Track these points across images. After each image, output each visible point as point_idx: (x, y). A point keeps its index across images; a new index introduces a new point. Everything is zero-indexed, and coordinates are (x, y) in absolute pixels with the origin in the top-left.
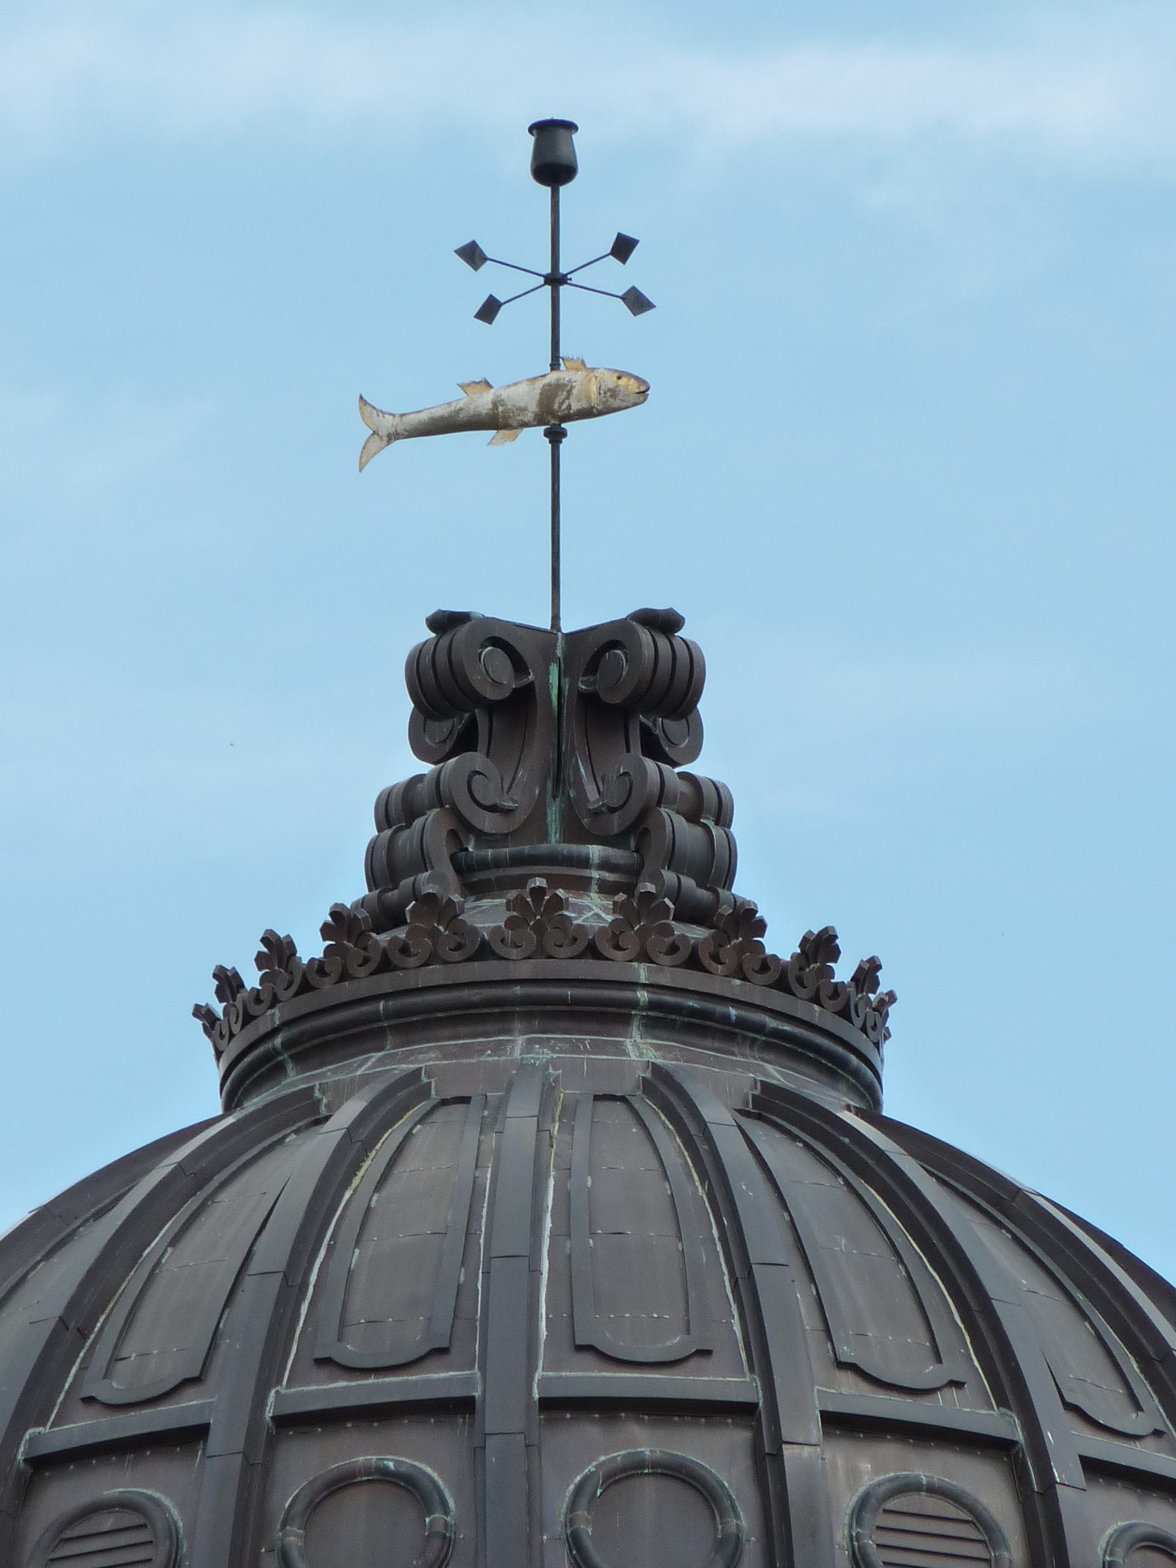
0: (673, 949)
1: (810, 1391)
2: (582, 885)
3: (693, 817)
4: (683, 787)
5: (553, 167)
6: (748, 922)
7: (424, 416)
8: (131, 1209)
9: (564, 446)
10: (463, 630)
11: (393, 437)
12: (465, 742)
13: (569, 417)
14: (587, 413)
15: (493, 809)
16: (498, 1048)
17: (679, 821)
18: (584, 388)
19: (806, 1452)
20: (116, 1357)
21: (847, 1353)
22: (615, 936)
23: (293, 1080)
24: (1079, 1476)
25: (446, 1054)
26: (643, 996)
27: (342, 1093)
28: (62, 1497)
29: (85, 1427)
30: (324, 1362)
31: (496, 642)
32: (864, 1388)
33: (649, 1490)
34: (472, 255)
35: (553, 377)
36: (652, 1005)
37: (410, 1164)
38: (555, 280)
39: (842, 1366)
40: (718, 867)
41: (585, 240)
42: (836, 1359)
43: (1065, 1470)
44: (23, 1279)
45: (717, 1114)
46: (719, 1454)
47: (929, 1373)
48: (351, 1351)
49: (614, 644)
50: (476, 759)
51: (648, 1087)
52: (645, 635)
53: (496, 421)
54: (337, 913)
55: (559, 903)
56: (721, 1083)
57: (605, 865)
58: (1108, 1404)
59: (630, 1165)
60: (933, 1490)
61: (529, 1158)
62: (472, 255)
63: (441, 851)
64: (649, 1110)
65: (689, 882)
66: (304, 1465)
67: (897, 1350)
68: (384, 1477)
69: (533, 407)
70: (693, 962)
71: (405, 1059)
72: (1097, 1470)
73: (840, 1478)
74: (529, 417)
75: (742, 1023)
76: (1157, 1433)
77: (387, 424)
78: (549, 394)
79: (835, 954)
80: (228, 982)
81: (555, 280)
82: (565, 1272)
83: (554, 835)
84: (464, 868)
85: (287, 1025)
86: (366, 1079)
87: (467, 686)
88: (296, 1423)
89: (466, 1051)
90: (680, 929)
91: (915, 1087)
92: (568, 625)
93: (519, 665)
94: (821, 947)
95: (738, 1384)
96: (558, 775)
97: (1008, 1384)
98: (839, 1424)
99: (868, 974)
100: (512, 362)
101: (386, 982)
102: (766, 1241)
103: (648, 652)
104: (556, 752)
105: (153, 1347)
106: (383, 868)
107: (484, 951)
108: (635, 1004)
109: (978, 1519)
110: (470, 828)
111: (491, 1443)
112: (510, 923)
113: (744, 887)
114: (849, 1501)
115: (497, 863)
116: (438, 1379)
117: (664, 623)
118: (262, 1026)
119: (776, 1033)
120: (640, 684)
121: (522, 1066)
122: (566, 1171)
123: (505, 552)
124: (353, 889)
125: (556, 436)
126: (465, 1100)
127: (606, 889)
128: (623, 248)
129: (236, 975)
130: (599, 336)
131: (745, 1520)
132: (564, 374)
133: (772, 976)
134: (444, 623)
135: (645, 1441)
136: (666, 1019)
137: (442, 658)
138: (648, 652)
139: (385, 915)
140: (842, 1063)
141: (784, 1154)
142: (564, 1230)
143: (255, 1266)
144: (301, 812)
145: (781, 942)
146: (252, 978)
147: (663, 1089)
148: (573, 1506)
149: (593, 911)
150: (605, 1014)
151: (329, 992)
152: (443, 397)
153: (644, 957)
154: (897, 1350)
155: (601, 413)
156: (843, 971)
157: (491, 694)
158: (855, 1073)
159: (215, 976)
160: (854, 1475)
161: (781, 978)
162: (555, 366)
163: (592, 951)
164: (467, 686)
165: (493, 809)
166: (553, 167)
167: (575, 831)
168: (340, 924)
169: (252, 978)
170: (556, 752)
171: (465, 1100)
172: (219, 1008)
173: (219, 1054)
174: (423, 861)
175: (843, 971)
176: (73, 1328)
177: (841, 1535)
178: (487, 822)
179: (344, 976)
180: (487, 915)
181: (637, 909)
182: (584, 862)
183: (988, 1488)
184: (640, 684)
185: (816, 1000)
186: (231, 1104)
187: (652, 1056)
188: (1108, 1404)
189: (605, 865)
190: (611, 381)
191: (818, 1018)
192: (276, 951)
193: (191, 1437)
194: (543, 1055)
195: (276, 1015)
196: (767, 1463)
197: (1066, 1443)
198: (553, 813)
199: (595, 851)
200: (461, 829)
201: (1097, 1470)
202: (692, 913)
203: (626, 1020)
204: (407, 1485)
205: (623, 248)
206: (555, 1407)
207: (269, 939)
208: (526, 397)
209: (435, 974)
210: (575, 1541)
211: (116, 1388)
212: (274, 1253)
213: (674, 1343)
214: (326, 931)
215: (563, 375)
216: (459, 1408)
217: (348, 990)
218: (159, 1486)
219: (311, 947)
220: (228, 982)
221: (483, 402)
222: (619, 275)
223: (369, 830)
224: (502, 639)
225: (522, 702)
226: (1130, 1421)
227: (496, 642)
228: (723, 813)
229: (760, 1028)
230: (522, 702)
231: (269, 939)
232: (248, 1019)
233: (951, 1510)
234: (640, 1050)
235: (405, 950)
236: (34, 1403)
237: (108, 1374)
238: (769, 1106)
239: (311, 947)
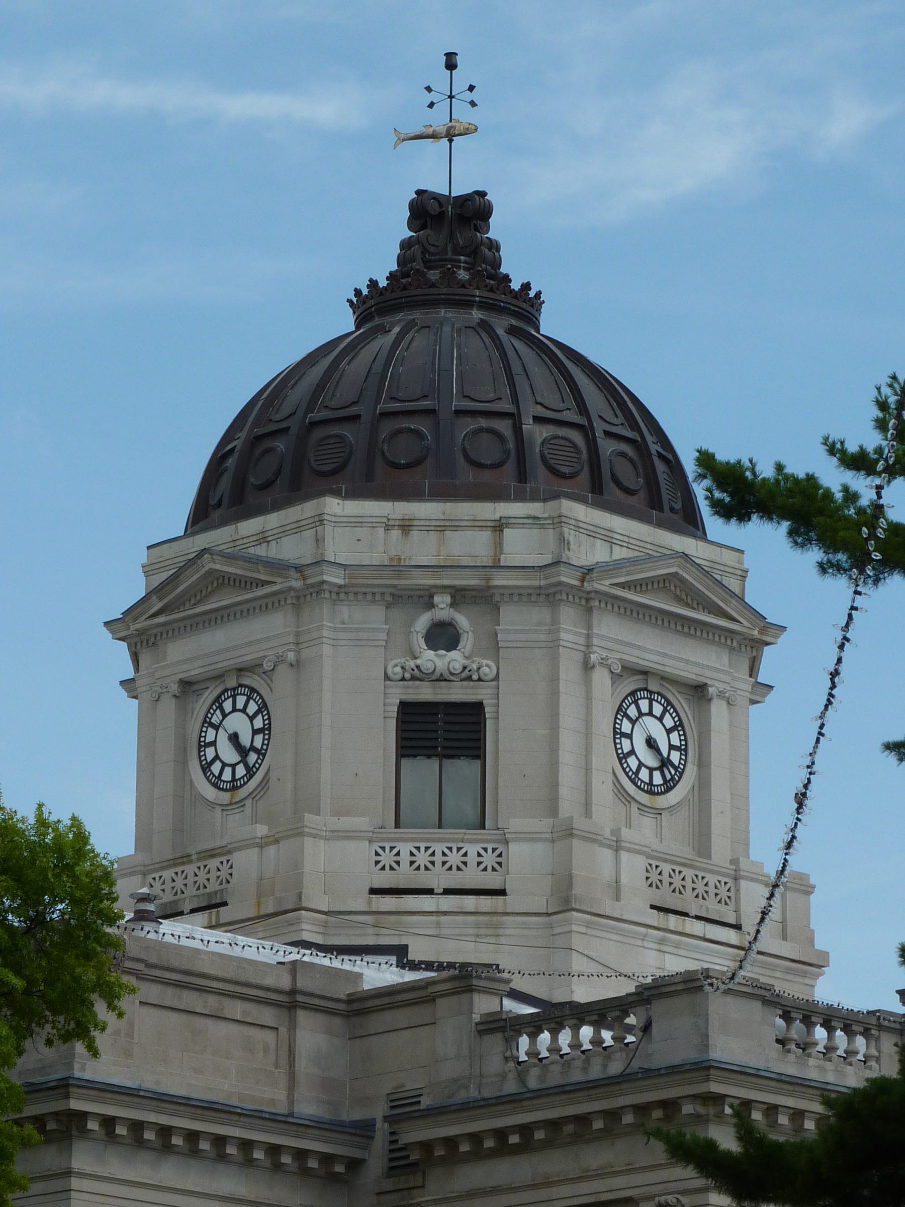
0: (486, 286)
1: (529, 410)
2: (459, 268)
3: (490, 250)
4: (487, 241)
5: (451, 63)
6: (507, 279)
8: (335, 353)
10: (425, 196)
11: (404, 140)
12: (423, 227)
14: (460, 135)
15: (433, 245)
16: (437, 313)
17: (487, 250)
18: (459, 128)
19: (528, 426)
20: (333, 396)
21: (539, 399)
22: (470, 282)
23: (377, 321)
24: (603, 436)
25: (422, 314)
26: (477, 299)
27: (393, 325)
28: (318, 433)
29: (325, 414)
30: (392, 398)
31: (434, 198)
32: (544, 410)
33: (485, 436)
34: (429, 89)
36: (480, 302)
37: (414, 344)
38: (451, 97)
39: (538, 403)
40: (497, 263)
41: (460, 86)
43: (599, 434)
44: (304, 374)
45: (500, 332)
46: (504, 426)
47: (561, 406)
48: (400, 395)
49: (469, 200)
50: (428, 231)
51: (479, 324)
52: (477, 198)
53: (434, 136)
54: (391, 273)
55: (455, 272)
56: (501, 324)
57: (465, 262)
58: (609, 416)
59: (476, 344)
60: (562, 438)
61: (450, 342)
62: (429, 89)
63: (419, 256)
64: (479, 330)
65: (489, 267)
66: (387, 427)
67: (552, 399)
68: (411, 430)
70: (491, 290)
71: (410, 315)
72: (607, 434)
73: (539, 434)
75: (504, 307)
76: (622, 424)
77: (402, 136)
79: (530, 289)
80: (358, 292)
81: (451, 97)
82: (460, 375)
83: (450, 253)
84: (425, 262)
85: (372, 305)
86: (400, 321)
87: (426, 211)
88: (385, 415)
89: (428, 313)
90: (488, 281)
91: (552, 325)
92: (453, 195)
93: (441, 205)
94: (526, 287)
95: (506, 406)
96: (451, 236)
97: (583, 409)
98: (538, 419)
99: (538, 295)
100: (439, 119)
101: (405, 293)
102: (516, 368)
103: (478, 202)
104: (450, 229)
105: (345, 392)
106: (401, 261)
107: (433, 285)
108: (475, 301)
109: (575, 446)
110: (427, 251)
111: (441, 422)
112: (440, 277)
113: (503, 270)
114: (540, 441)
115: (435, 261)
116: (425, 404)
117: (483, 194)
118: (368, 305)
119: (514, 311)
120: (473, 210)
121: (444, 318)
122: (459, 348)
123: (436, 172)
124: (394, 267)
125: (451, 141)
126: (429, 327)
127: (465, 269)
128: (471, 88)
130: (464, 115)
131: (511, 445)
133: (513, 294)
134: (420, 193)
135: (483, 423)
136: (483, 306)
137: (419, 202)
138: (478, 202)
139: (406, 275)
140: (531, 320)
141: (517, 344)
142: (460, 363)
143: (373, 371)
145: (515, 286)
146: (365, 292)
147: (484, 325)
148: (464, 440)
149: (463, 275)
150: (467, 304)
151: (389, 295)
152: (419, 129)
153: (478, 288)
154: (552, 399)
156: (532, 294)
157: (434, 213)
158: (534, 323)
160: (541, 434)
161: (515, 295)
162: (451, 121)
163: (463, 286)
164: (426, 211)
165: (433, 245)
166: (451, 63)
167: (457, 251)
168: (392, 277)
169: (365, 292)
170: (450, 229)
171: (429, 327)
172: (355, 300)
173: (354, 313)
174: (414, 260)
175: (532, 294)
176: (320, 387)
177: (537, 450)
178: (432, 249)
179: (392, 292)
180: (434, 275)
181: (477, 276)
182: (460, 261)
183: (577, 437)
184: (473, 210)
185: (525, 302)
186: (358, 327)
187: (480, 316)
188: (609, 416)
189: (465, 262)
190: (467, 126)
191: (525, 306)
192: (373, 284)
193: (356, 418)
194: (449, 315)
195: (373, 302)
196: (517, 429)
197: (599, 427)
198: (449, 247)
199: (462, 258)
200: (425, 251)
201: (607, 434)
202: (491, 277)
203: (472, 306)
205: (471, 88)
206: (459, 413)
207: (371, 280)
208: (442, 130)
209: (419, 291)
210: (464, 450)
211: (334, 403)
212: (378, 367)
213: (491, 396)
214: (388, 278)
215: (453, 123)
216: (431, 412)
217: (393, 295)
218: (346, 431)
219: (383, 283)
220: (358, 292)
221: (430, 131)
222: (469, 96)
223: (398, 251)
224: (436, 197)
225: (441, 215)
226: (615, 421)
227: (434, 198)
228: (498, 249)
229: (509, 309)
230: (441, 215)
231: (371, 280)
232: (364, 303)
233: (568, 444)
234: (476, 315)
235: (410, 284)
236: (310, 408)
237: (331, 400)
238: (513, 331)
239: (383, 283)
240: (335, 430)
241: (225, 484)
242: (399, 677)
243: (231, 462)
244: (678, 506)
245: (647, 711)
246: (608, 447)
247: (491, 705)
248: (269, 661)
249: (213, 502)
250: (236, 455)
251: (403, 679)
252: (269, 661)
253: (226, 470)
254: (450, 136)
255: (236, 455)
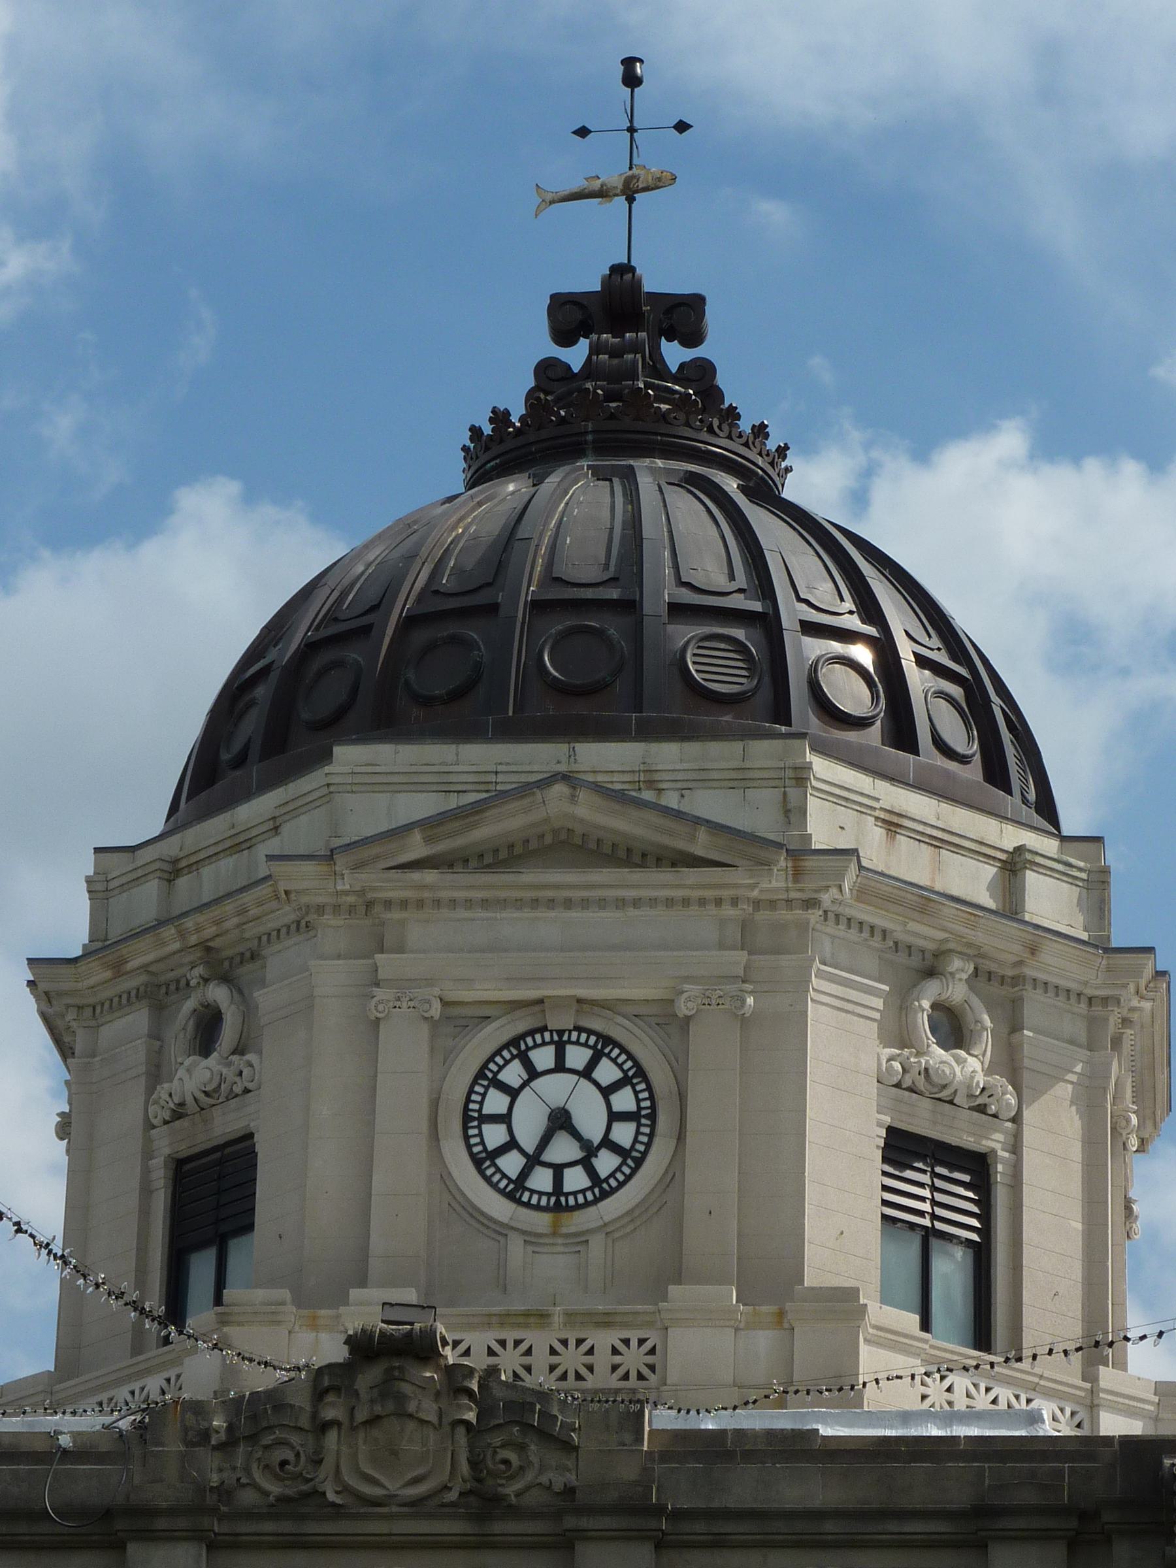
5: (632, 80)
7: (566, 193)
9: (634, 205)
11: (552, 202)
13: (637, 192)
14: (646, 189)
19: (791, 636)
35: (630, 173)
42: (111, 980)
53: (603, 193)
69: (620, 187)
74: (618, 191)
77: (549, 197)
78: (628, 181)
79: (767, 436)
80: (475, 432)
85: (499, 451)
94: (760, 431)
125: (631, 200)
129: (480, 428)
132: (635, 171)
144: (505, 363)
146: (487, 429)
152: (577, 183)
155: (653, 189)
159: (470, 430)
162: (631, 168)
166: (632, 80)
169: (487, 429)
185: (760, 454)
192: (500, 417)
204: (598, 633)
215: (635, 171)
220: (475, 432)
221: (596, 185)
239: (517, 411)
240: (452, 628)
241: (251, 726)
242: (895, 1080)
243: (261, 692)
244: (1032, 796)
245: (507, 1099)
246: (917, 680)
247: (1005, 1162)
248: (689, 999)
249: (225, 756)
250: (274, 676)
251: (898, 1085)
252: (689, 999)
253: (252, 703)
254: (630, 192)
255: (274, 676)
